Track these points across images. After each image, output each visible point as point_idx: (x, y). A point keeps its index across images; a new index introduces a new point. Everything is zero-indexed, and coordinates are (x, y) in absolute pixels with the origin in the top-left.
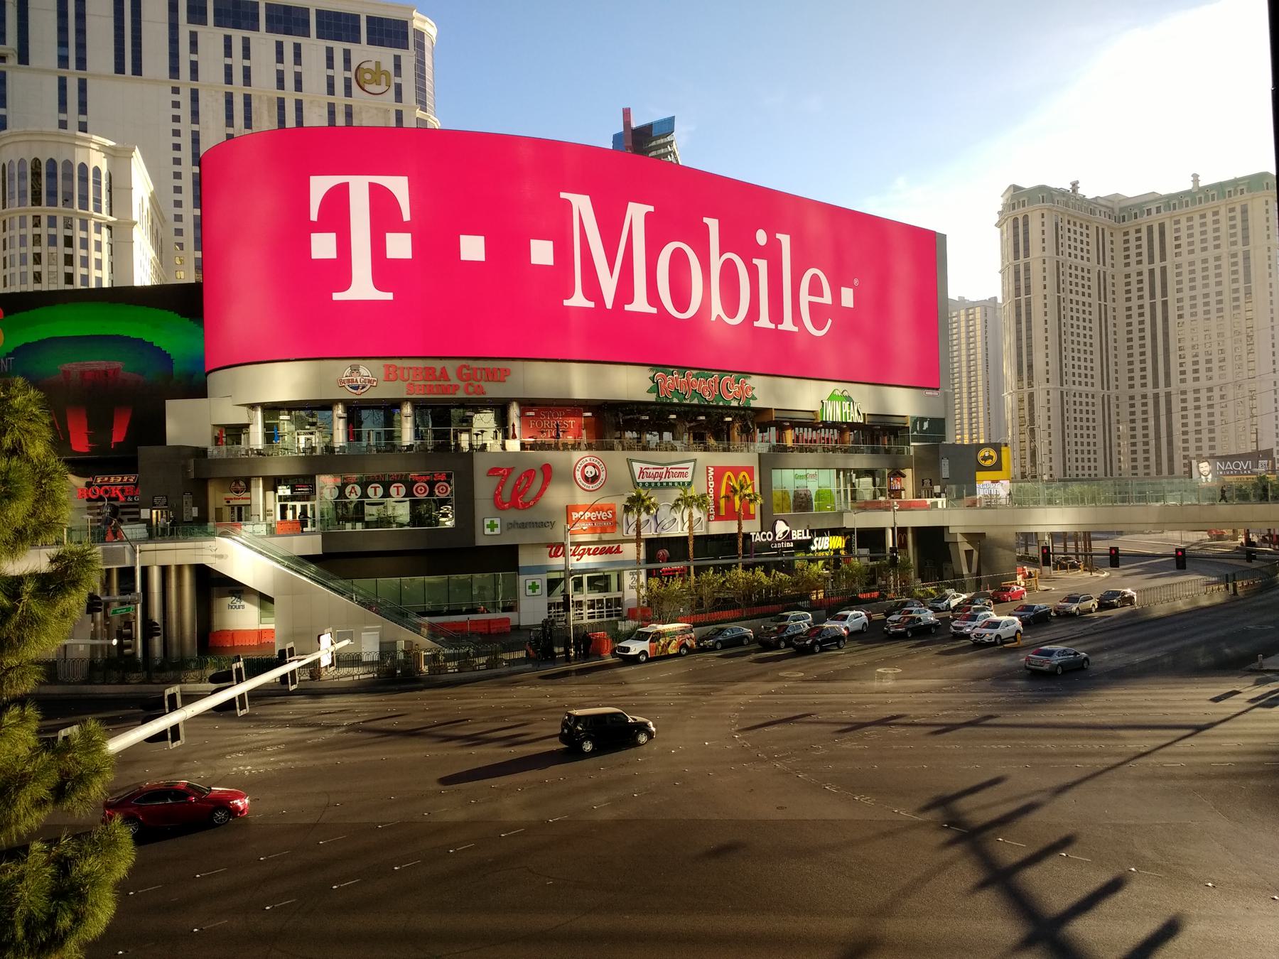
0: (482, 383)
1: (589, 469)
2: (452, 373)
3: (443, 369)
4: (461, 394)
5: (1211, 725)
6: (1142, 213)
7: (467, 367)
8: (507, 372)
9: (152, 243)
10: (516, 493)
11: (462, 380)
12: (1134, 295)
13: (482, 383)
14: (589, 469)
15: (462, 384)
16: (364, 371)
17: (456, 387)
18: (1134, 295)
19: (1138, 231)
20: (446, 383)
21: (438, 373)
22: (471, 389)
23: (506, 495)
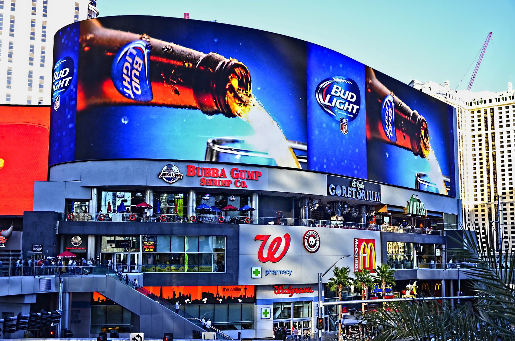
0: (245, 181)
1: (312, 239)
2: (228, 173)
3: (223, 170)
4: (232, 187)
5: (229, 339)
6: (481, 102)
7: (236, 170)
8: (259, 174)
9: (438, 159)
10: (272, 253)
11: (234, 178)
12: (506, 154)
13: (245, 181)
14: (312, 239)
15: (233, 181)
16: (175, 169)
17: (230, 182)
18: (506, 154)
19: (479, 112)
20: (224, 179)
21: (219, 173)
22: (238, 184)
23: (265, 255)
